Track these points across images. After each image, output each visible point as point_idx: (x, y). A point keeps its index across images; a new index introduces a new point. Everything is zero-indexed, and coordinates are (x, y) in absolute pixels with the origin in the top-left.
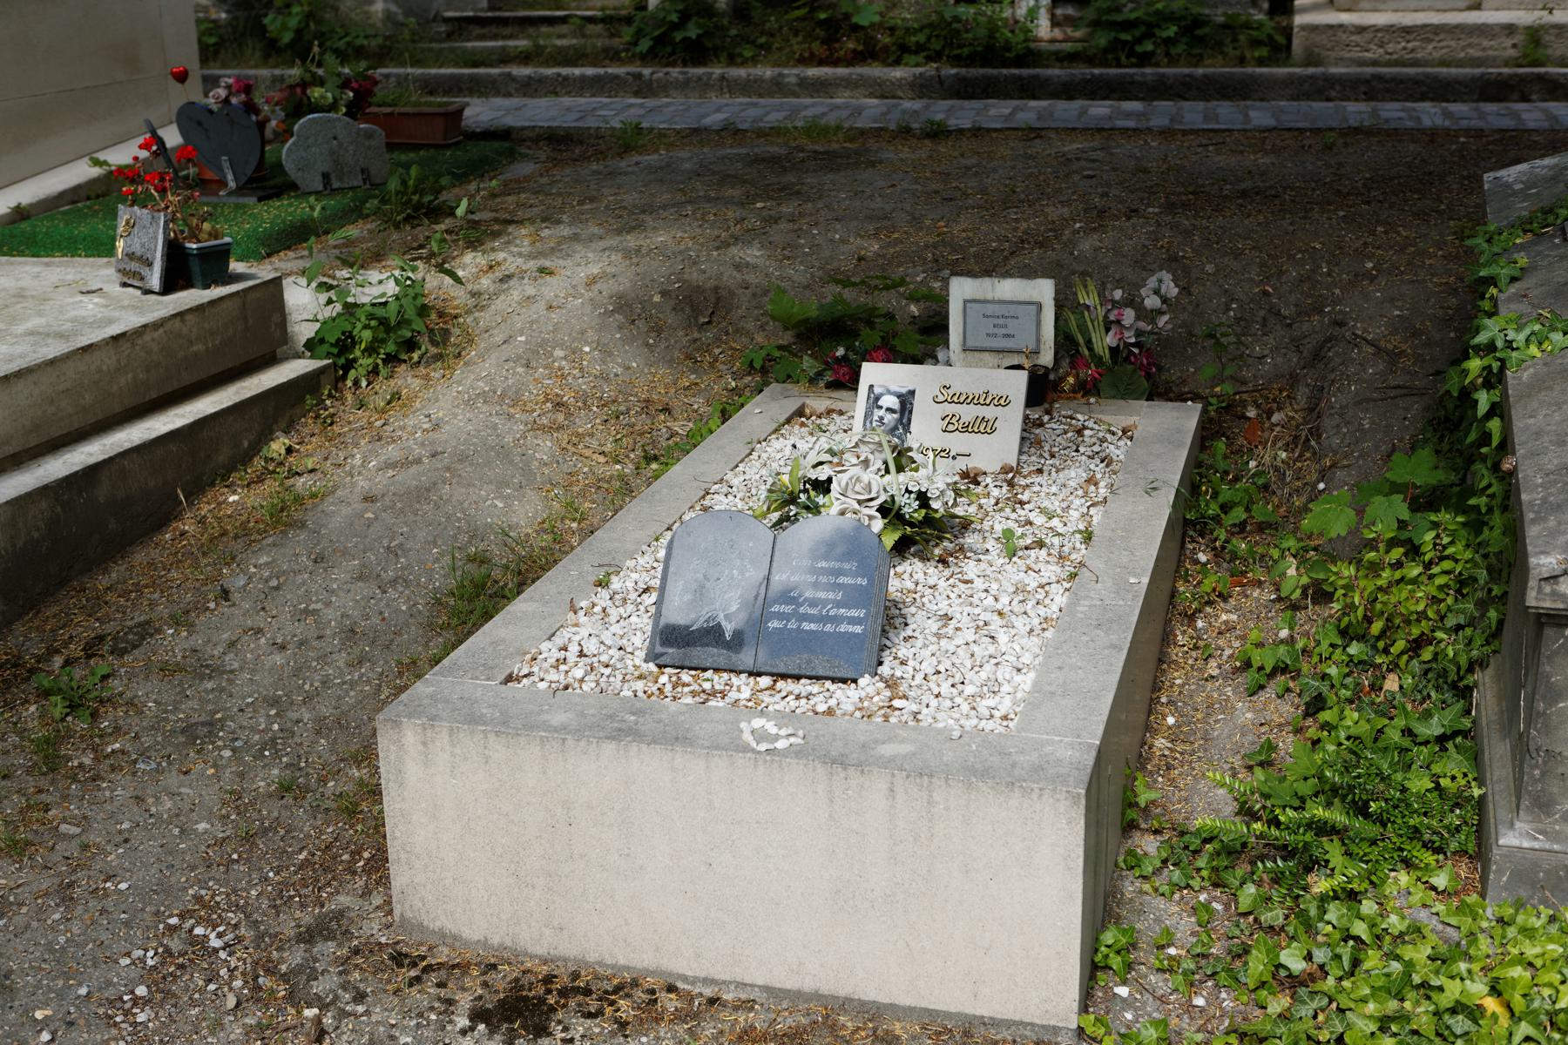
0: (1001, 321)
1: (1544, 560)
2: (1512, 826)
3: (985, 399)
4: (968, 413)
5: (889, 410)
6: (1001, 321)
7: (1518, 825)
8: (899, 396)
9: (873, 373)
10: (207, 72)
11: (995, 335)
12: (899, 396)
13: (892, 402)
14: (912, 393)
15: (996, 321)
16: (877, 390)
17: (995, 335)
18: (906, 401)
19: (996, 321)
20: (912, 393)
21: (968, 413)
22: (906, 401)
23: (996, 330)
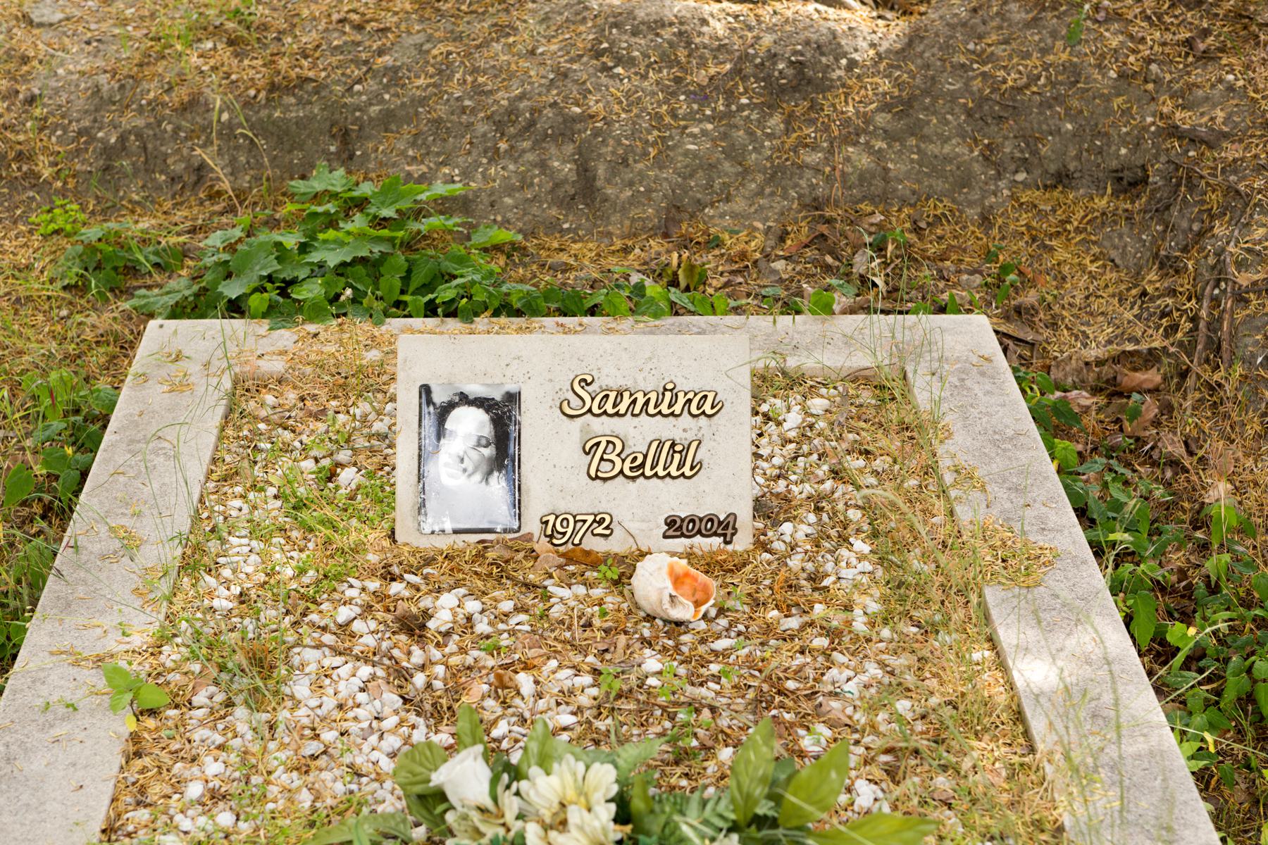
3: (666, 402)
4: (640, 433)
14: (513, 398)
20: (513, 398)
21: (640, 433)
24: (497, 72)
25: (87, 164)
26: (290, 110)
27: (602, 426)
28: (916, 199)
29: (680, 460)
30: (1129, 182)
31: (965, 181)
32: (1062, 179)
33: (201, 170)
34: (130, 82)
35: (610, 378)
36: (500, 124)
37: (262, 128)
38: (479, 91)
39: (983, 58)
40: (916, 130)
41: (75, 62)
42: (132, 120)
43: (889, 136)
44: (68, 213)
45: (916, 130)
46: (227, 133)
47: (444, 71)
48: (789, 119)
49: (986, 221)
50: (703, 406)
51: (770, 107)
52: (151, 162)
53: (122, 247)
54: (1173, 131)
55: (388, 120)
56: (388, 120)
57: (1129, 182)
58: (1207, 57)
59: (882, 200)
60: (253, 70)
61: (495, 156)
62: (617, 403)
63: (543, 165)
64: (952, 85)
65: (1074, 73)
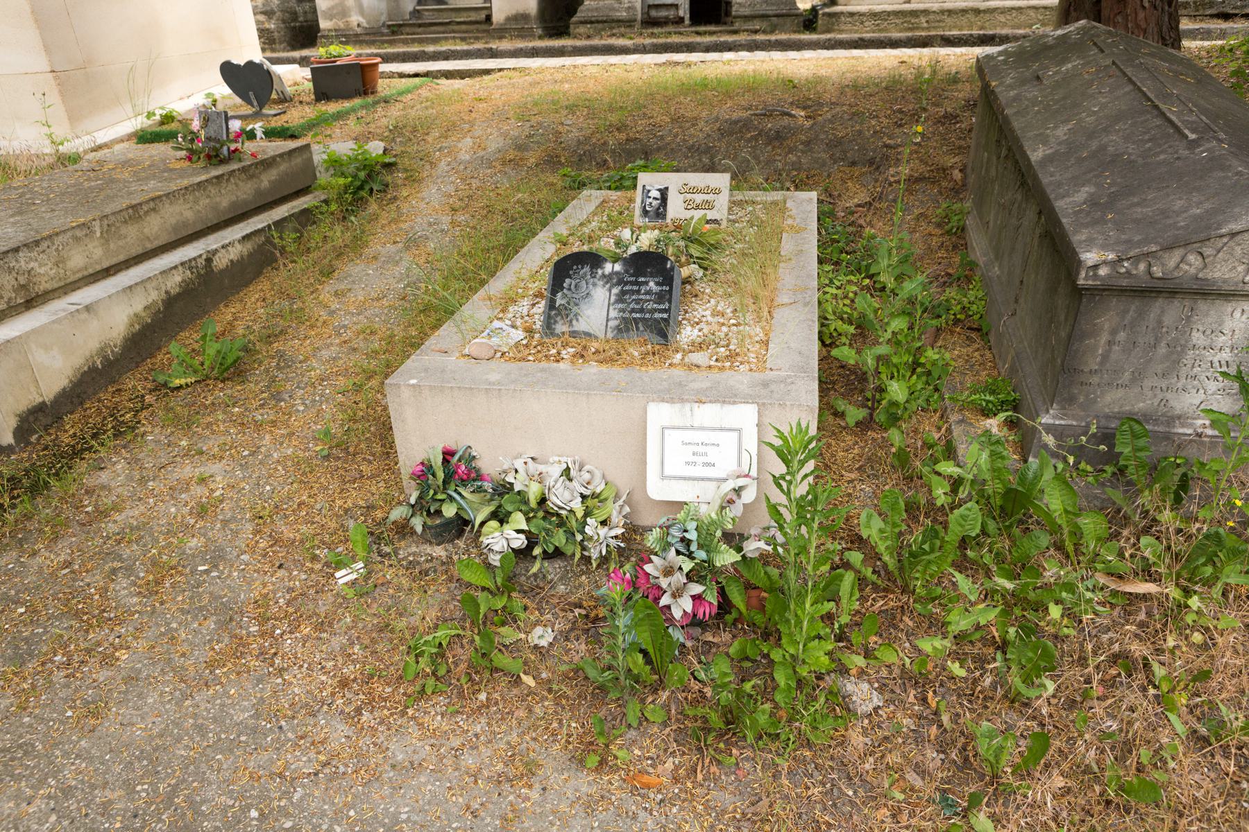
0: (701, 449)
1: (1089, 255)
2: (1047, 412)
3: (707, 190)
4: (699, 198)
5: (655, 199)
6: (701, 449)
7: (1051, 412)
8: (659, 190)
9: (644, 178)
10: (739, 196)
11: (695, 463)
12: (659, 190)
13: (657, 194)
14: (667, 188)
15: (696, 449)
16: (648, 188)
17: (695, 463)
18: (664, 193)
19: (696, 449)
20: (667, 188)
21: (699, 198)
22: (664, 193)
23: (695, 459)
24: (690, 136)
25: (575, 159)
26: (632, 146)
27: (689, 196)
28: (809, 169)
29: (709, 205)
30: (871, 162)
31: (824, 164)
32: (853, 164)
33: (606, 161)
34: (587, 139)
35: (692, 184)
36: (689, 149)
37: (623, 150)
38: (684, 140)
39: (833, 129)
40: (811, 150)
41: (575, 134)
42: (587, 147)
43: (803, 152)
44: (568, 170)
45: (811, 150)
46: (613, 151)
47: (676, 136)
48: (774, 148)
49: (829, 176)
50: (717, 192)
51: (767, 144)
52: (592, 158)
53: (731, 502)
54: (887, 146)
55: (659, 149)
56: (659, 149)
57: (871, 162)
58: (901, 126)
59: (799, 170)
60: (623, 136)
61: (687, 157)
62: (695, 190)
63: (700, 160)
64: (822, 136)
65: (860, 132)
